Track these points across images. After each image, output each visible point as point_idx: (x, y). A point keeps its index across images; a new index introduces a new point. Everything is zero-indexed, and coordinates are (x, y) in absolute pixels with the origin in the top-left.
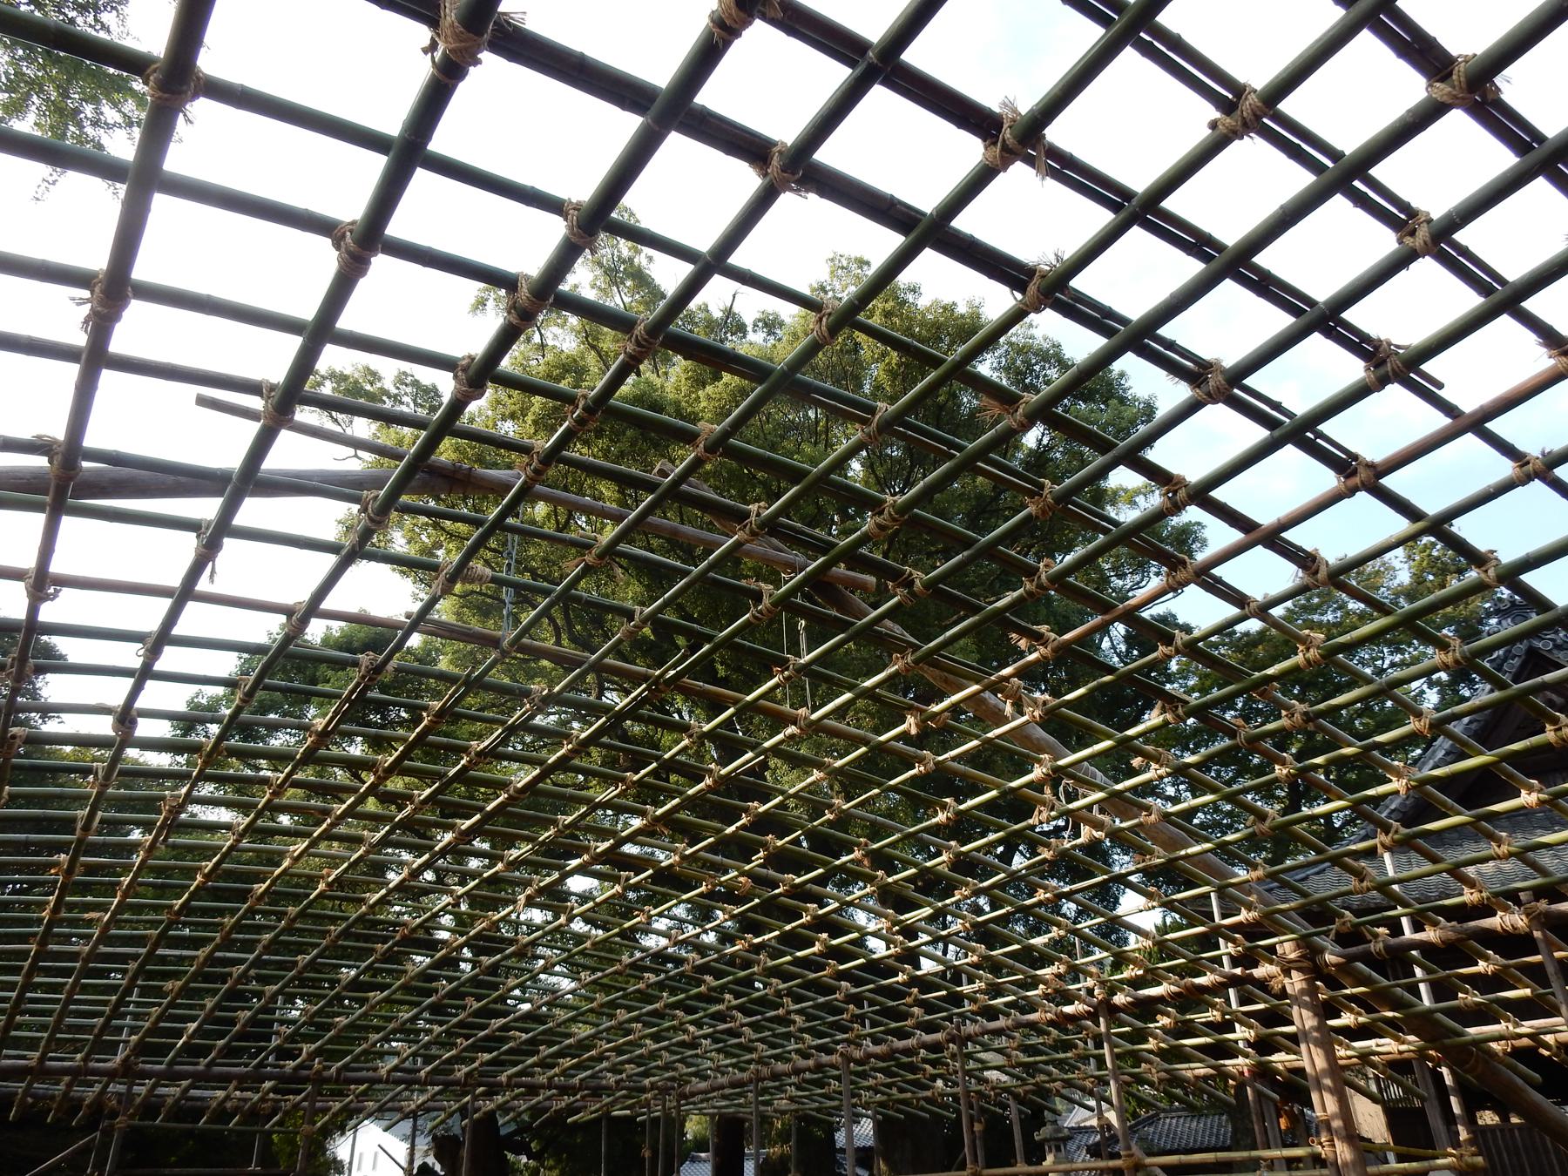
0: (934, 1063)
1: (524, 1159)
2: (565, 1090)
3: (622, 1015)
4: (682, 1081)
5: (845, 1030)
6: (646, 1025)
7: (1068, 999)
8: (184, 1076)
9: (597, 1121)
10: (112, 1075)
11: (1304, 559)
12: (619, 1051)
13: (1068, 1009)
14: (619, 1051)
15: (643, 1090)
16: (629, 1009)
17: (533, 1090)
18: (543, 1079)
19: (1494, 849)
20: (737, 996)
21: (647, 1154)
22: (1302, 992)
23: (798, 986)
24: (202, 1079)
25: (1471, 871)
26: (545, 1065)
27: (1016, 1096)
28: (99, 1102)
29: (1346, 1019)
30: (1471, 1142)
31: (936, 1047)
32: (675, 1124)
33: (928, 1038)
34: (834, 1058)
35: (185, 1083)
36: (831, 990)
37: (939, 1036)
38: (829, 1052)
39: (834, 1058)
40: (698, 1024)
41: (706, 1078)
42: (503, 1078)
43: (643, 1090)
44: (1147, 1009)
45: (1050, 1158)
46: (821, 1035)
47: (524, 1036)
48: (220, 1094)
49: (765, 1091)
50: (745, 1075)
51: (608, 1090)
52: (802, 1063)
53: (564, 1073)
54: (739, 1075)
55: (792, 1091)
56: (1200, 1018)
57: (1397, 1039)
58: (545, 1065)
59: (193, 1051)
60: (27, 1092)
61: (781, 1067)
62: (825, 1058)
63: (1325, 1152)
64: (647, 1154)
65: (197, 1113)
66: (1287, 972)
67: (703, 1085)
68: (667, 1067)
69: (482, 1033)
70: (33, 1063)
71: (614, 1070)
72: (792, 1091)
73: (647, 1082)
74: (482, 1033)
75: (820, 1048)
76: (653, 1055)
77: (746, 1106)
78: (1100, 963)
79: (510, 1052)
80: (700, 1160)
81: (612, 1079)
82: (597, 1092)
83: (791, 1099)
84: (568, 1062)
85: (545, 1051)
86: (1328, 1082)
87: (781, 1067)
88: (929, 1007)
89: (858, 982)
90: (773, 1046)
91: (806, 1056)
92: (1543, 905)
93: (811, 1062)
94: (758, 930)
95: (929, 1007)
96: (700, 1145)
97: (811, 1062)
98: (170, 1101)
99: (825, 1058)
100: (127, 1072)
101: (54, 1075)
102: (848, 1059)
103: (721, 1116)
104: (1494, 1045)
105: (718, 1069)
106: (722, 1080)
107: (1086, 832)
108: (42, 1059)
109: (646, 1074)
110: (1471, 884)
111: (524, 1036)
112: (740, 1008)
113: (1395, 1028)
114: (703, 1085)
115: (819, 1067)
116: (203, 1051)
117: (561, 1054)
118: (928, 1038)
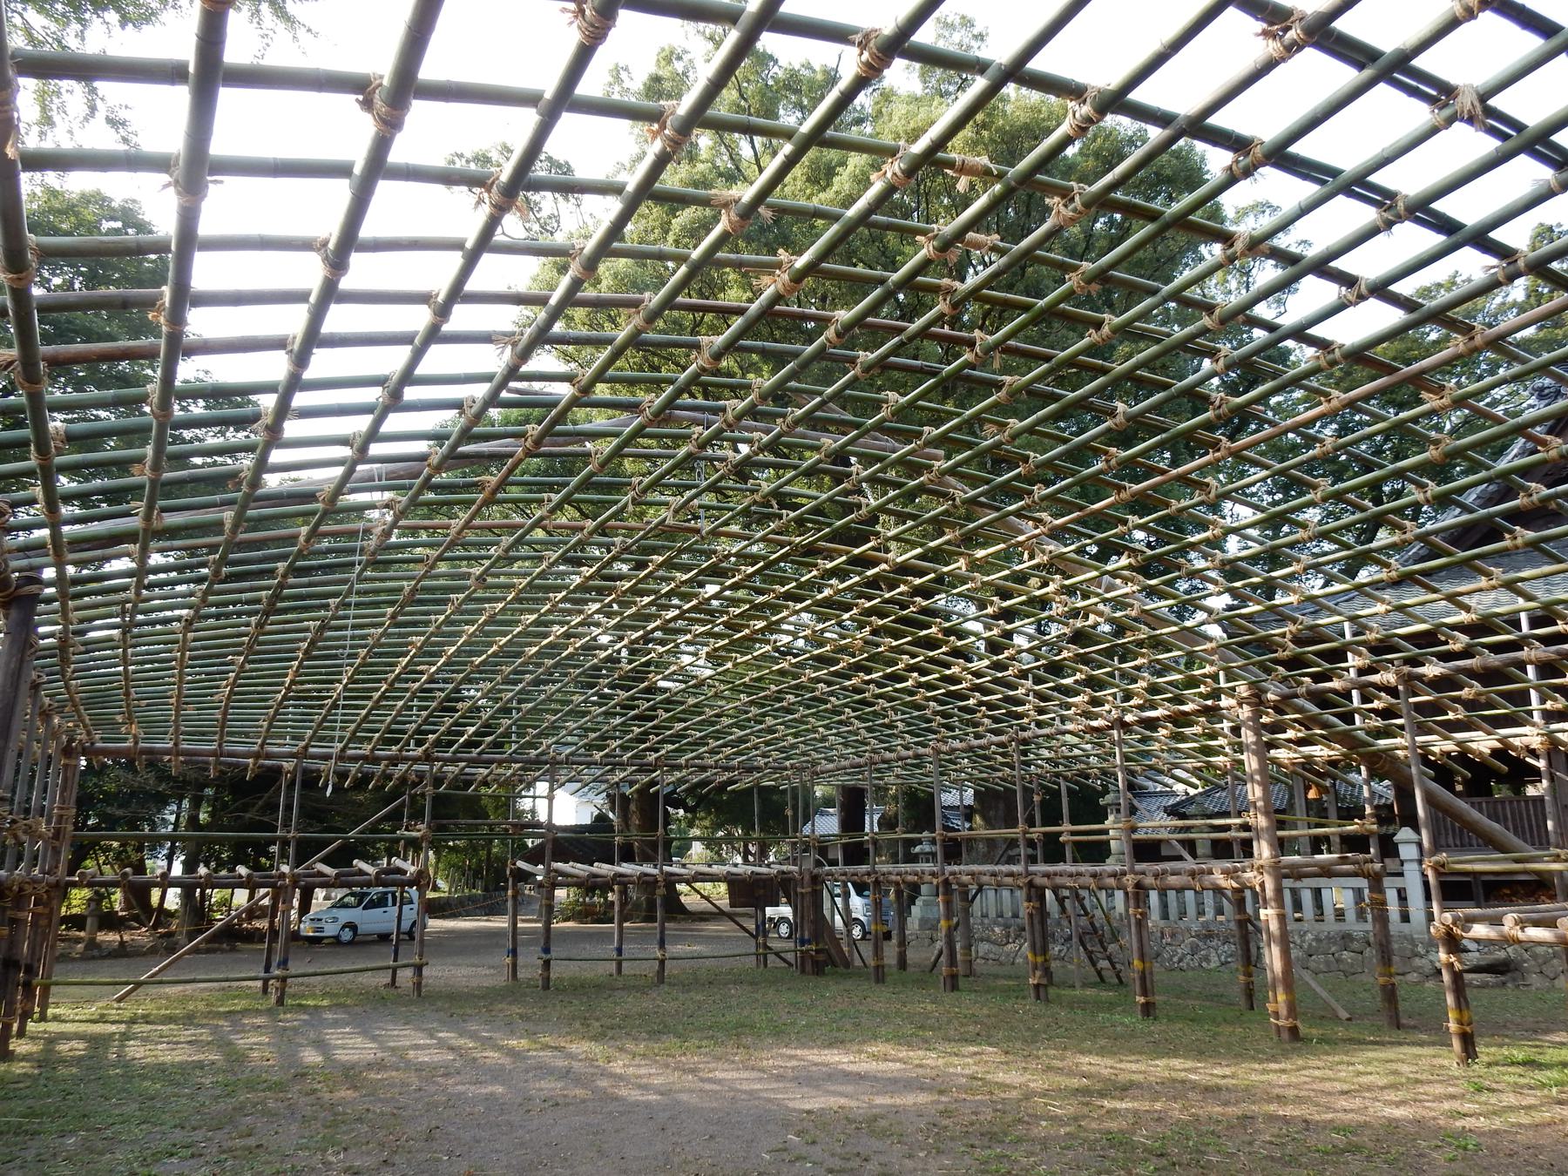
0: (1003, 755)
1: (681, 812)
2: (726, 769)
3: (770, 721)
4: (814, 763)
5: (935, 732)
6: (788, 727)
7: (1096, 717)
8: (461, 760)
9: (751, 789)
10: (416, 760)
11: (1323, 344)
12: (767, 744)
13: (1094, 723)
14: (767, 744)
15: (786, 769)
16: (775, 718)
17: (703, 769)
18: (711, 762)
19: (1483, 582)
20: (854, 710)
21: (789, 813)
22: (1249, 719)
23: (917, 557)
24: (473, 762)
25: (1465, 600)
26: (713, 752)
27: (1066, 778)
28: (403, 780)
29: (1290, 734)
30: (1371, 815)
31: (1001, 745)
32: (808, 792)
33: (995, 739)
34: (927, 750)
35: (463, 764)
36: (924, 708)
37: (1003, 738)
38: (925, 746)
39: (927, 750)
40: (827, 727)
41: (833, 761)
42: (682, 761)
43: (786, 769)
44: (1151, 724)
45: (1111, 818)
46: (918, 736)
47: (699, 734)
48: (486, 772)
49: (878, 771)
50: (862, 760)
51: (759, 769)
52: (904, 753)
53: (727, 758)
54: (858, 760)
55: (899, 771)
56: (1187, 731)
57: (1329, 747)
58: (713, 752)
59: (470, 744)
60: (359, 770)
61: (888, 755)
62: (921, 750)
63: (1251, 821)
64: (789, 813)
65: (468, 784)
66: (1240, 705)
67: (831, 766)
68: (804, 754)
69: (545, 642)
70: (367, 753)
71: (764, 756)
72: (899, 771)
73: (787, 763)
74: (545, 642)
75: (916, 744)
76: (793, 746)
77: (863, 781)
78: (1114, 695)
79: (689, 744)
80: (828, 814)
81: (762, 761)
82: (750, 770)
83: (898, 776)
84: (728, 751)
85: (713, 743)
86: (1257, 777)
87: (888, 755)
88: (995, 720)
89: (942, 703)
90: (882, 742)
91: (907, 749)
92: (1407, 669)
93: (910, 753)
94: (869, 671)
95: (995, 720)
96: (828, 802)
97: (910, 753)
98: (450, 776)
99: (921, 750)
100: (428, 758)
101: (377, 761)
102: (938, 752)
103: (844, 787)
104: (1399, 752)
105: (842, 756)
106: (844, 763)
107: (1092, 617)
108: (372, 750)
109: (787, 759)
110: (1468, 609)
111: (699, 734)
112: (856, 718)
113: (1327, 740)
114: (831, 766)
115: (917, 756)
116: (477, 745)
117: (725, 746)
118: (995, 739)
